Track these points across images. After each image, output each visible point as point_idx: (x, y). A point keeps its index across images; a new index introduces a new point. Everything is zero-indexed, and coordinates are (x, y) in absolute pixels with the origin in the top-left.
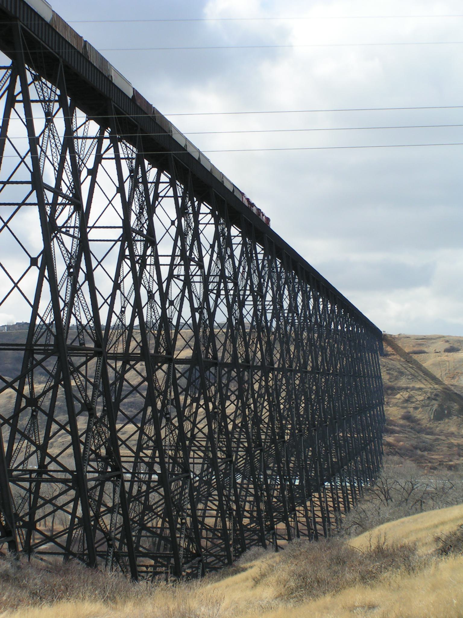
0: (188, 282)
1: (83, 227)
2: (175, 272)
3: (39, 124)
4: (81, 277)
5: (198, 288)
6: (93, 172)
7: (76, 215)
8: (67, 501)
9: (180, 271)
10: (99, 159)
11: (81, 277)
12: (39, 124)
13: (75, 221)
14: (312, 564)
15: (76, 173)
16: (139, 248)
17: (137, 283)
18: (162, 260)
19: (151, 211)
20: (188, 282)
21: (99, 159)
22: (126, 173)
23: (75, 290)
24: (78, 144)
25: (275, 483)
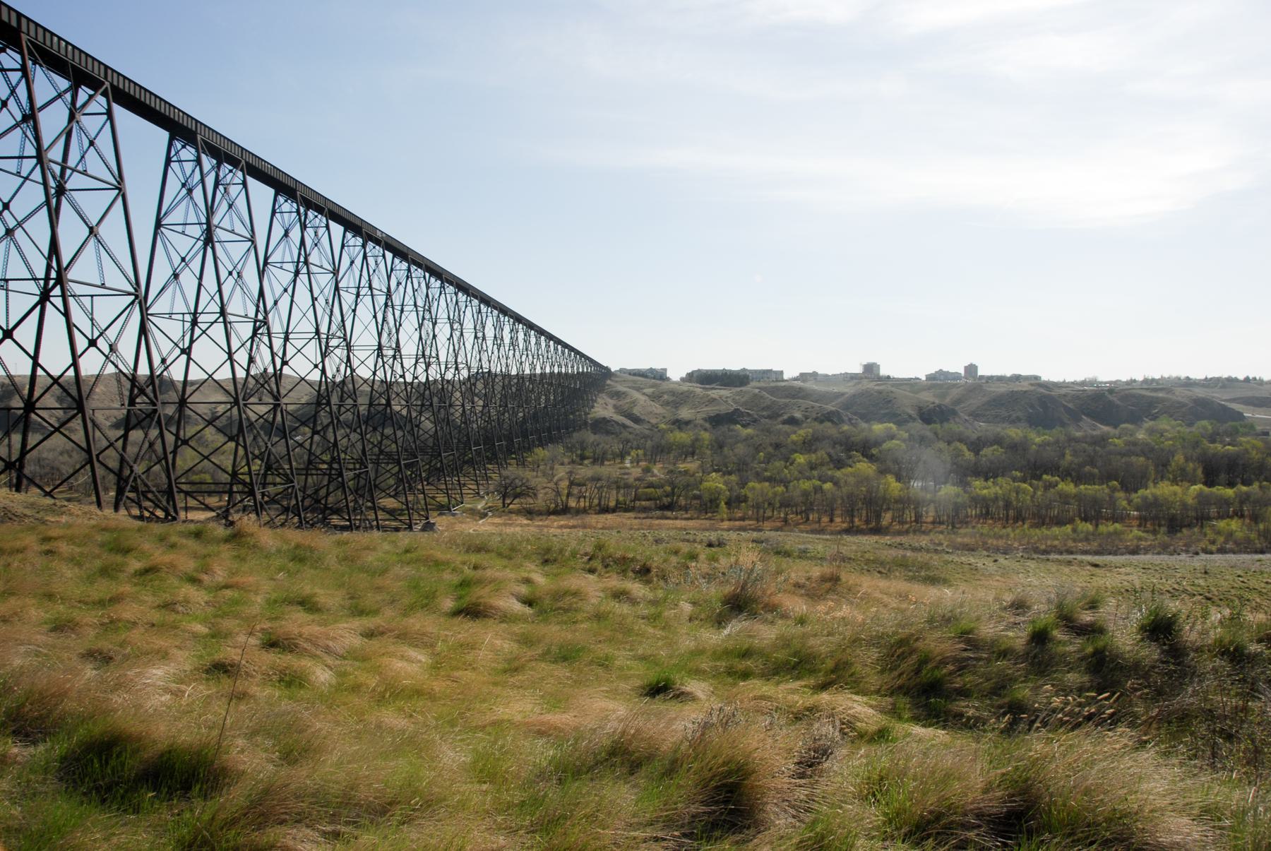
0: (527, 356)
1: (462, 329)
2: (455, 327)
3: (449, 300)
4: (462, 344)
5: (530, 357)
6: (464, 312)
7: (284, 252)
8: (51, 437)
9: (511, 348)
10: (466, 306)
11: (462, 344)
12: (449, 300)
13: (459, 327)
14: (228, 624)
15: (459, 311)
16: (499, 342)
17: (499, 350)
18: (419, 309)
19: (502, 330)
20: (527, 356)
21: (466, 306)
22: (474, 311)
23: (459, 348)
24: (459, 304)
25: (325, 428)
